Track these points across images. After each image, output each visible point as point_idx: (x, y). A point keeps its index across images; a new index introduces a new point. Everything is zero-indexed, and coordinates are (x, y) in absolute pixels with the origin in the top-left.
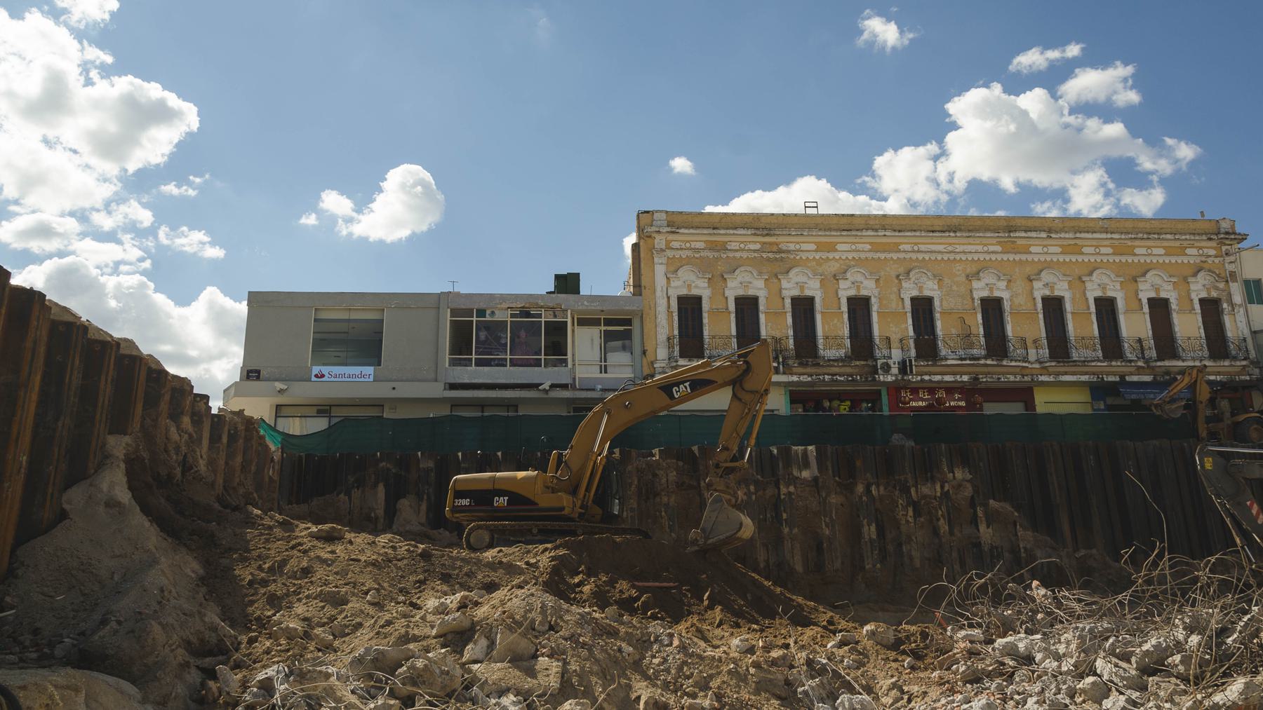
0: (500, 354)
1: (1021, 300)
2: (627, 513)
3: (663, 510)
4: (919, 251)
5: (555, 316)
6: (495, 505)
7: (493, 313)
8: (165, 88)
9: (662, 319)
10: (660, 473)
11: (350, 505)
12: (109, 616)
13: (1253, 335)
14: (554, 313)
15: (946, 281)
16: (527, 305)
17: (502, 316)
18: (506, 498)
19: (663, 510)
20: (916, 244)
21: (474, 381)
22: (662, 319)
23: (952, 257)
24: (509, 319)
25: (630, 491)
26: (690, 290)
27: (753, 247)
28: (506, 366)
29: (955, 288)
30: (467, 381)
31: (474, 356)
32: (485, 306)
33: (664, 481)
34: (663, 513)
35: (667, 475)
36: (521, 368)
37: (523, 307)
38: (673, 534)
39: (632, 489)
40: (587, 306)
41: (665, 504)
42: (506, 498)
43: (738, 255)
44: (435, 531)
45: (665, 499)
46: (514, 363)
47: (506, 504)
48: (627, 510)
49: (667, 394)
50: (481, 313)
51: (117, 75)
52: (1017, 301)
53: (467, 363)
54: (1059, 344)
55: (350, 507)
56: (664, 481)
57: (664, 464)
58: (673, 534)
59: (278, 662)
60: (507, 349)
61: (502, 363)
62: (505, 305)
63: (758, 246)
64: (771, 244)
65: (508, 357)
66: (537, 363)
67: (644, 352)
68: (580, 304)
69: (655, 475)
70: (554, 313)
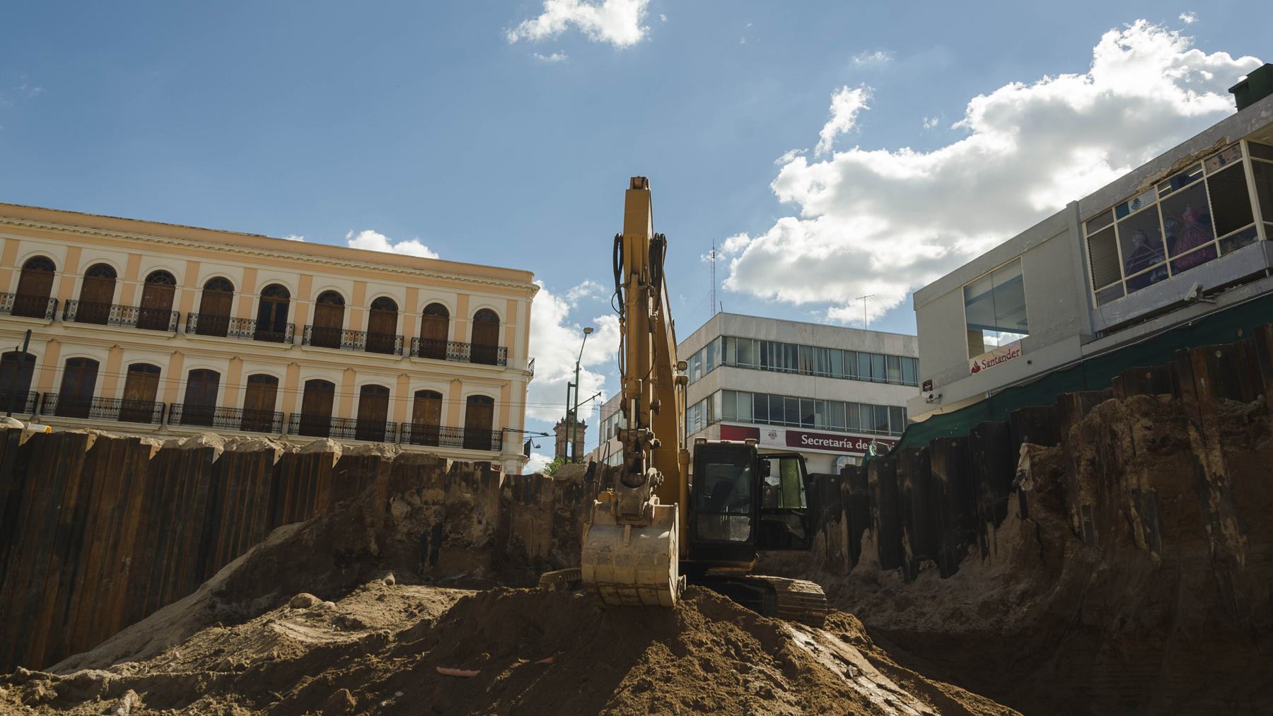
0: (1156, 261)
2: (1080, 518)
3: (1132, 504)
5: (1223, 162)
7: (1137, 201)
8: (987, 94)
10: (1119, 427)
11: (826, 543)
12: (38, 682)
14: (1220, 157)
16: (1176, 166)
17: (1153, 199)
19: (1132, 504)
21: (1128, 318)
24: (1158, 201)
25: (1079, 473)
28: (1166, 277)
30: (1119, 320)
31: (1124, 279)
32: (1121, 198)
33: (1126, 443)
34: (1133, 511)
35: (1131, 430)
36: (1197, 268)
37: (1172, 173)
38: (1154, 554)
39: (1082, 469)
40: (1266, 118)
41: (1133, 491)
44: (460, 596)
45: (1133, 481)
46: (1178, 268)
48: (1078, 513)
49: (1002, 285)
50: (1122, 208)
51: (1205, 52)
53: (1118, 293)
56: (1126, 443)
57: (1124, 409)
58: (1154, 554)
60: (1163, 250)
62: (1147, 183)
65: (1168, 261)
66: (1210, 254)
68: (1253, 121)
69: (1114, 435)
70: (1220, 157)
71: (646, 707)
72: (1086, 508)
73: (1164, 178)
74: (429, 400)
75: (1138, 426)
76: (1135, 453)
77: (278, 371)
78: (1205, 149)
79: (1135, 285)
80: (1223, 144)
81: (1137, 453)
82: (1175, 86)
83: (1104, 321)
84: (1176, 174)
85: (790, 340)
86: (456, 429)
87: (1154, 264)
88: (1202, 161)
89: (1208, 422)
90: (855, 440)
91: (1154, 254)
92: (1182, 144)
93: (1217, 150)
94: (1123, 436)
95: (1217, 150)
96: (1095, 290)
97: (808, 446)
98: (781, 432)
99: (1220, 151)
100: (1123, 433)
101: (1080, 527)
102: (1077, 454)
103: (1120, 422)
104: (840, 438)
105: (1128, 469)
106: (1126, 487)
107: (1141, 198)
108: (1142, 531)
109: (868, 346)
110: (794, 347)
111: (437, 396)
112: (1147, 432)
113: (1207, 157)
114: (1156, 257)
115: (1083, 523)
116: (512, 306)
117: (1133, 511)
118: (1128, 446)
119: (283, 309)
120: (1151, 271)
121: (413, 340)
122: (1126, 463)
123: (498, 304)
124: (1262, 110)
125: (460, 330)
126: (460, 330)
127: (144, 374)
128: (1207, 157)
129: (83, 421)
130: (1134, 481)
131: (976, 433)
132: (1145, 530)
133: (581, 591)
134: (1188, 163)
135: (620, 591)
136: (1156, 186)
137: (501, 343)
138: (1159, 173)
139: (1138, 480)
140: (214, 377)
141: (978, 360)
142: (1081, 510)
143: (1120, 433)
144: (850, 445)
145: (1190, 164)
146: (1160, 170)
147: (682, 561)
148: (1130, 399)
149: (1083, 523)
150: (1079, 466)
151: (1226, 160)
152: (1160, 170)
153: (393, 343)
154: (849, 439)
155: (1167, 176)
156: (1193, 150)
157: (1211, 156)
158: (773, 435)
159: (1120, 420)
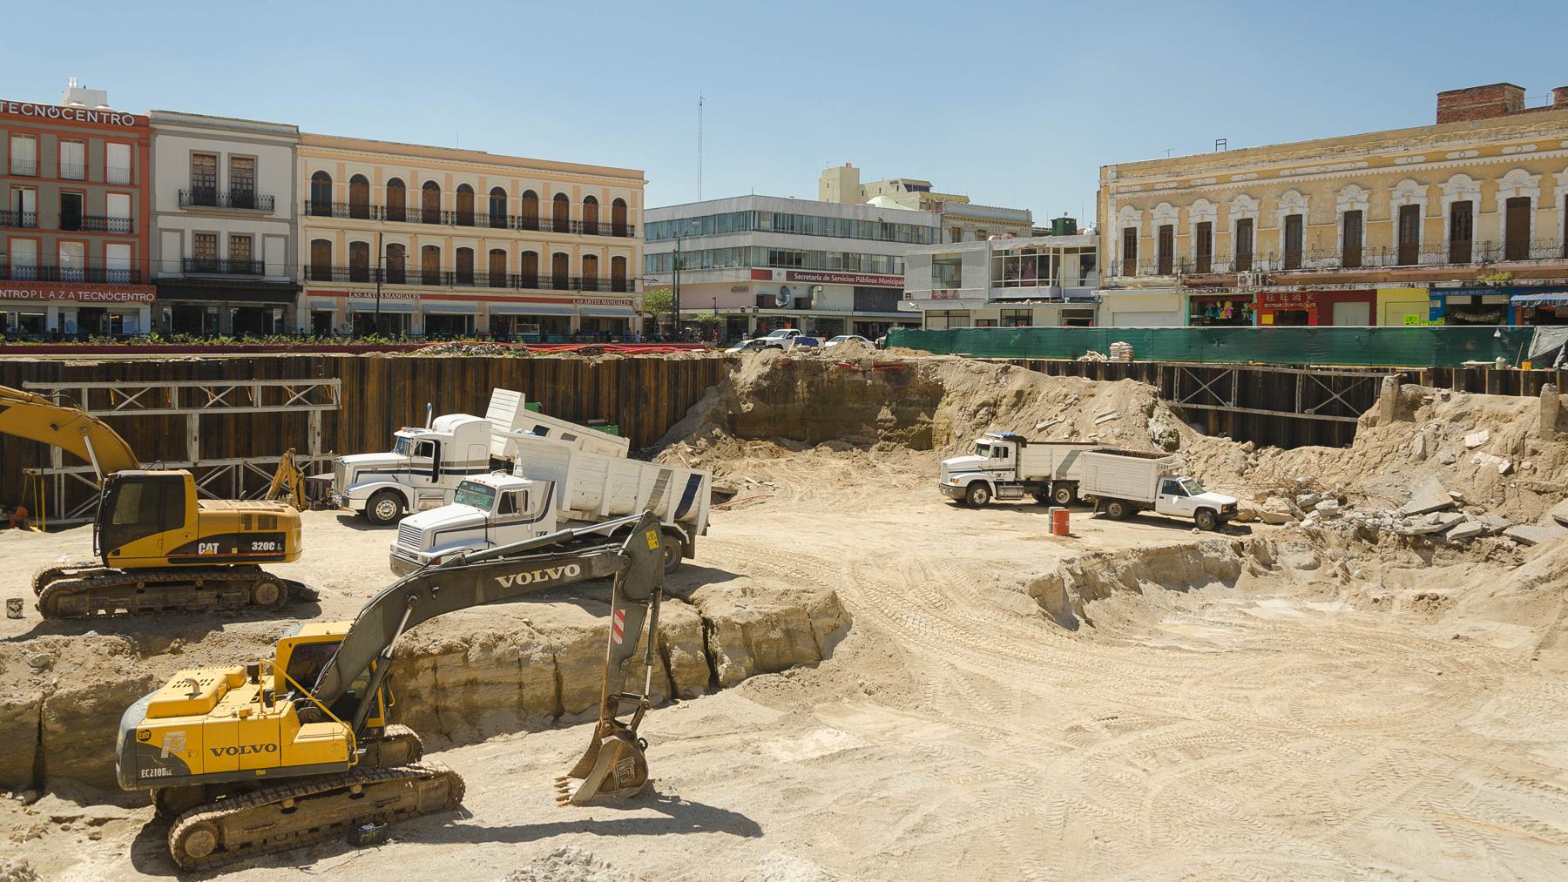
1: (1377, 211)
4: (1296, 175)
6: (200, 553)
9: (1112, 247)
13: (566, 717)
15: (1316, 198)
18: (216, 545)
20: (1293, 168)
22: (1112, 247)
23: (1322, 176)
26: (1243, 214)
27: (1171, 185)
29: (1322, 205)
42: (216, 545)
43: (1161, 192)
46: (1023, 284)
47: (216, 552)
52: (1374, 212)
54: (1408, 251)
55: (656, 422)
59: (128, 641)
61: (1016, 285)
63: (1175, 185)
64: (1185, 181)
66: (1033, 284)
67: (1101, 271)
74: (561, 259)
77: (471, 244)
82: (815, 600)
85: (790, 212)
86: (484, 274)
89: (915, 590)
90: (823, 275)
96: (997, 484)
97: (798, 280)
98: (784, 271)
104: (815, 274)
109: (834, 214)
110: (793, 216)
111: (503, 253)
116: (634, 195)
119: (503, 203)
121: (519, 218)
123: (625, 195)
125: (605, 214)
126: (605, 214)
127: (359, 249)
129: (366, 285)
137: (629, 222)
140: (470, 252)
141: (947, 249)
144: (820, 279)
147: (504, 384)
153: (568, 226)
154: (820, 274)
158: (779, 274)
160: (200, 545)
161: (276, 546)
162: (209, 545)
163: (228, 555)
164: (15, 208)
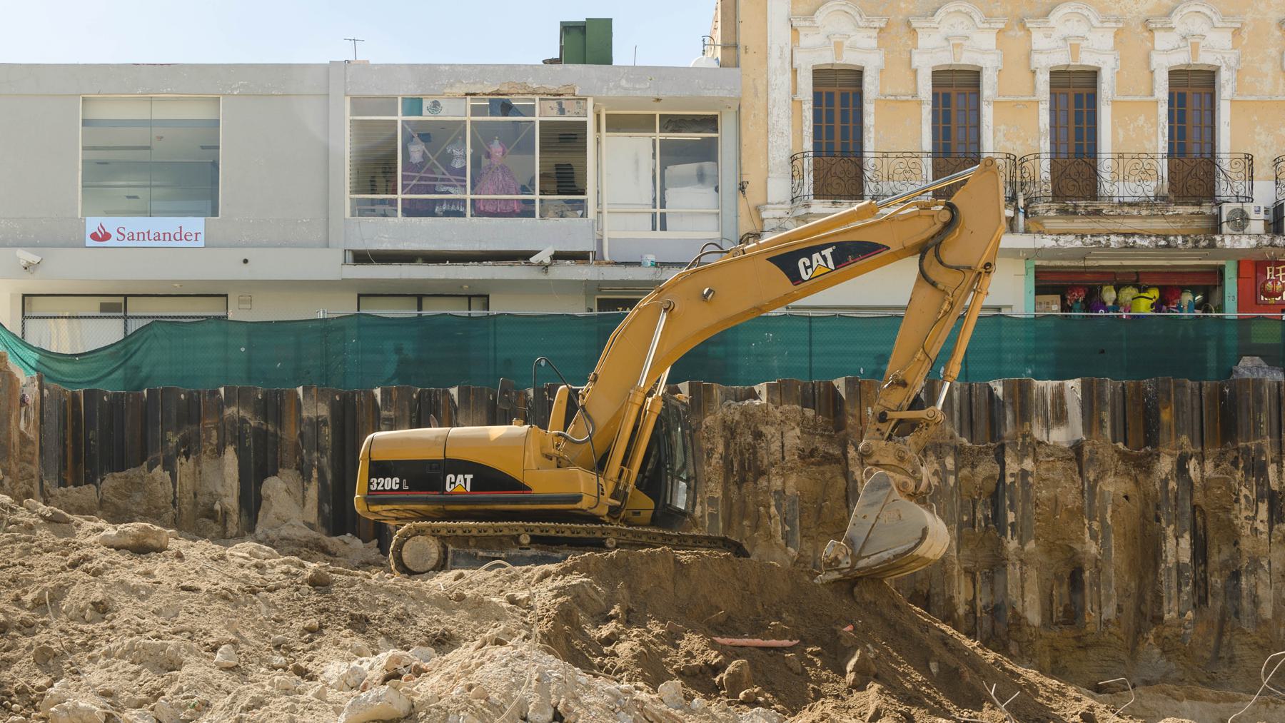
0: (451, 189)
3: (773, 503)
7: (436, 104)
18: (469, 477)
19: (773, 503)
24: (469, 119)
31: (400, 196)
34: (773, 510)
39: (714, 461)
41: (776, 492)
42: (469, 477)
46: (479, 211)
53: (386, 209)
57: (779, 415)
66: (526, 211)
70: (560, 104)
71: (682, 652)
72: (712, 501)
73: (484, 94)
75: (793, 433)
76: (783, 458)
78: (547, 86)
79: (412, 210)
80: (569, 91)
81: (787, 458)
83: (363, 240)
84: (500, 97)
87: (448, 193)
88: (537, 98)
91: (449, 180)
92: (519, 65)
93: (560, 95)
94: (773, 440)
95: (560, 95)
99: (561, 97)
100: (773, 437)
101: (702, 516)
102: (710, 446)
103: (771, 425)
105: (774, 471)
106: (768, 487)
107: (443, 103)
108: (780, 528)
112: (798, 441)
113: (545, 97)
114: (454, 186)
115: (707, 513)
117: (773, 510)
118: (776, 450)
120: (442, 200)
122: (772, 465)
124: (622, 78)
128: (545, 97)
130: (779, 483)
131: (546, 393)
132: (783, 527)
133: (1077, 546)
134: (520, 92)
135: (784, 545)
136: (469, 97)
138: (479, 86)
139: (784, 483)
142: (706, 500)
143: (769, 437)
145: (522, 94)
146: (483, 83)
148: (786, 407)
149: (707, 513)
150: (709, 457)
151: (566, 111)
152: (483, 83)
155: (489, 94)
156: (530, 79)
157: (549, 97)
159: (773, 424)
160: (449, 477)
161: (401, 484)
162: (460, 477)
163: (1259, 293)
164: (149, 209)
